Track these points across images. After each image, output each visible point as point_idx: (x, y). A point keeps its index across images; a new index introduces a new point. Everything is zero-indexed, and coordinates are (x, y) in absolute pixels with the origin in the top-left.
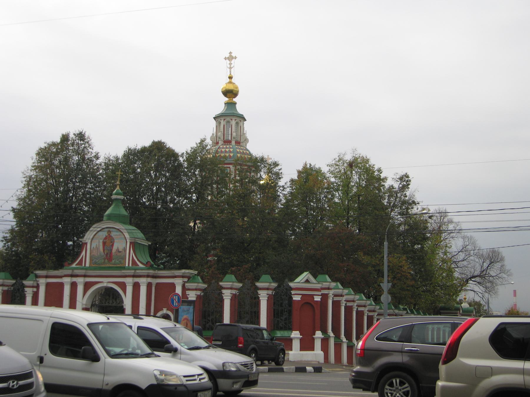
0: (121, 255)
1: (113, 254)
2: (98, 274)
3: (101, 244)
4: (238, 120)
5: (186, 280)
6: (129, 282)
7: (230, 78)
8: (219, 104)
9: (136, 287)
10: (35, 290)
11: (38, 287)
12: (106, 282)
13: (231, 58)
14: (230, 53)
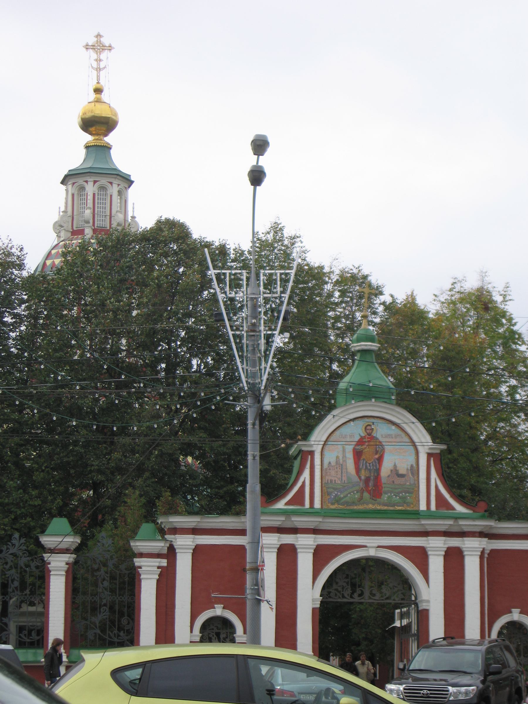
0: (407, 483)
1: (383, 480)
3: (350, 456)
4: (123, 185)
6: (436, 546)
7: (98, 91)
8: (74, 149)
9: (454, 559)
10: (164, 562)
11: (171, 553)
12: (371, 548)
14: (99, 36)
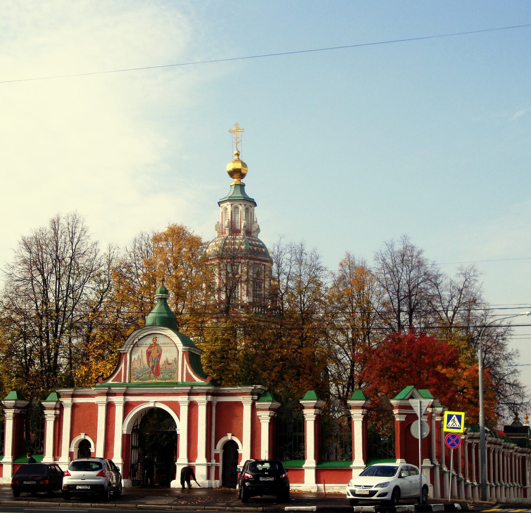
1: (161, 367)
2: (141, 392)
3: (145, 355)
4: (249, 204)
5: (256, 397)
6: (183, 400)
7: (238, 155)
9: (192, 406)
11: (61, 408)
12: (151, 402)
13: (237, 130)
